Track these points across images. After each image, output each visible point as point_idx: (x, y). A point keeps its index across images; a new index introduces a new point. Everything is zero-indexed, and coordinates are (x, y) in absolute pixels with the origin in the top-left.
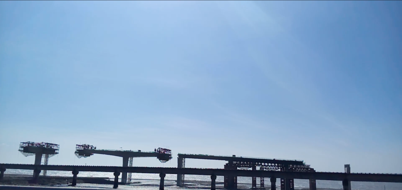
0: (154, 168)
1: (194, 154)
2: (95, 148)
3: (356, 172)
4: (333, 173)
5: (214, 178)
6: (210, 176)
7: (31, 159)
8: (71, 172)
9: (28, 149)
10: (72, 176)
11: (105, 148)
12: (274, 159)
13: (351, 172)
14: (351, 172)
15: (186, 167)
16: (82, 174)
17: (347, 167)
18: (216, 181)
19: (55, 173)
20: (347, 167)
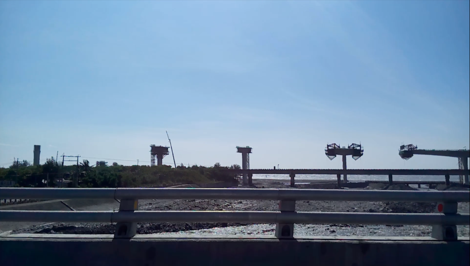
0: (302, 170)
1: (147, 165)
2: (416, 148)
3: (350, 169)
4: (433, 170)
5: (447, 178)
6: (336, 175)
7: (337, 163)
8: (289, 175)
9: (332, 151)
10: (290, 178)
11: (437, 148)
12: (217, 166)
13: (347, 169)
14: (347, 169)
15: (250, 168)
16: (396, 178)
17: (275, 167)
18: (295, 178)
19: (323, 177)
20: (275, 167)
